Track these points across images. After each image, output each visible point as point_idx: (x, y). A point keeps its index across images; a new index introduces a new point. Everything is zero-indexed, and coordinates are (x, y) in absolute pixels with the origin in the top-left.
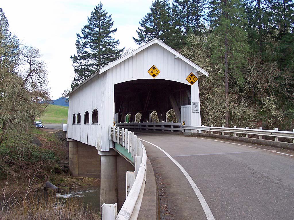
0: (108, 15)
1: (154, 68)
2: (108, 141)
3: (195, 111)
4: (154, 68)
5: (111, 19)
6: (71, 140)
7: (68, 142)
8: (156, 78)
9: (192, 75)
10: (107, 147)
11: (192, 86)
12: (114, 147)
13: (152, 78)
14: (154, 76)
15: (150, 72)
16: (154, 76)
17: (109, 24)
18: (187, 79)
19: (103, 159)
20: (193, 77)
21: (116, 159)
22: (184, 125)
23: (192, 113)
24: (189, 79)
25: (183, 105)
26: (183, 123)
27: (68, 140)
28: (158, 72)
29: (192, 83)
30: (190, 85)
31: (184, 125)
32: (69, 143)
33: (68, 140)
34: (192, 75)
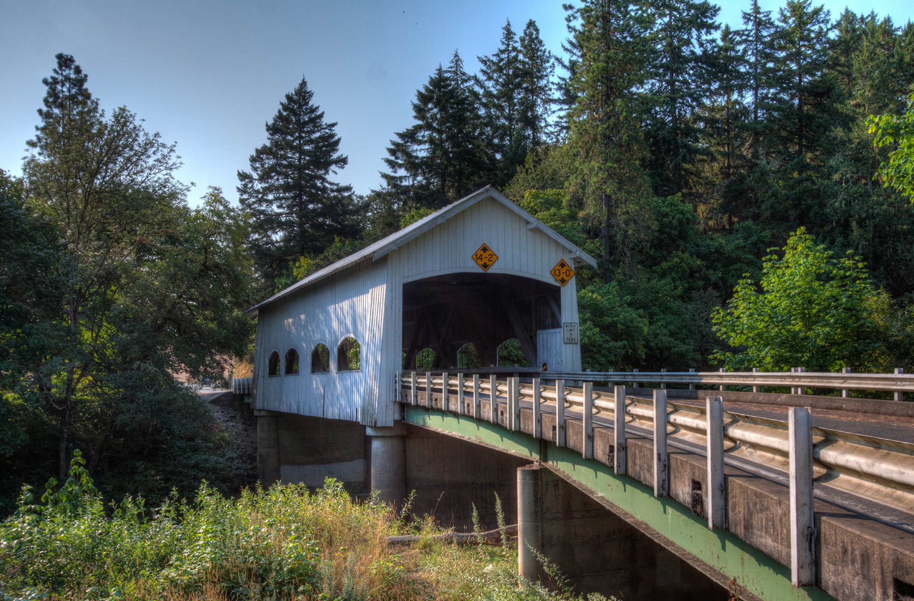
0: (326, 120)
1: (485, 249)
2: (391, 406)
3: (571, 341)
4: (485, 249)
5: (103, 111)
6: (263, 413)
7: (256, 417)
8: (493, 270)
9: (562, 265)
10: (388, 417)
11: (563, 289)
12: (403, 418)
13: (480, 270)
14: (485, 266)
15: (477, 258)
16: (485, 266)
17: (329, 143)
18: (554, 273)
19: (376, 445)
20: (564, 270)
21: (405, 443)
22: (545, 370)
23: (564, 346)
24: (557, 272)
25: (540, 329)
26: (543, 366)
27: (256, 413)
28: (493, 257)
29: (563, 281)
30: (558, 284)
31: (545, 370)
32: (260, 421)
33: (256, 413)
34: (562, 265)
